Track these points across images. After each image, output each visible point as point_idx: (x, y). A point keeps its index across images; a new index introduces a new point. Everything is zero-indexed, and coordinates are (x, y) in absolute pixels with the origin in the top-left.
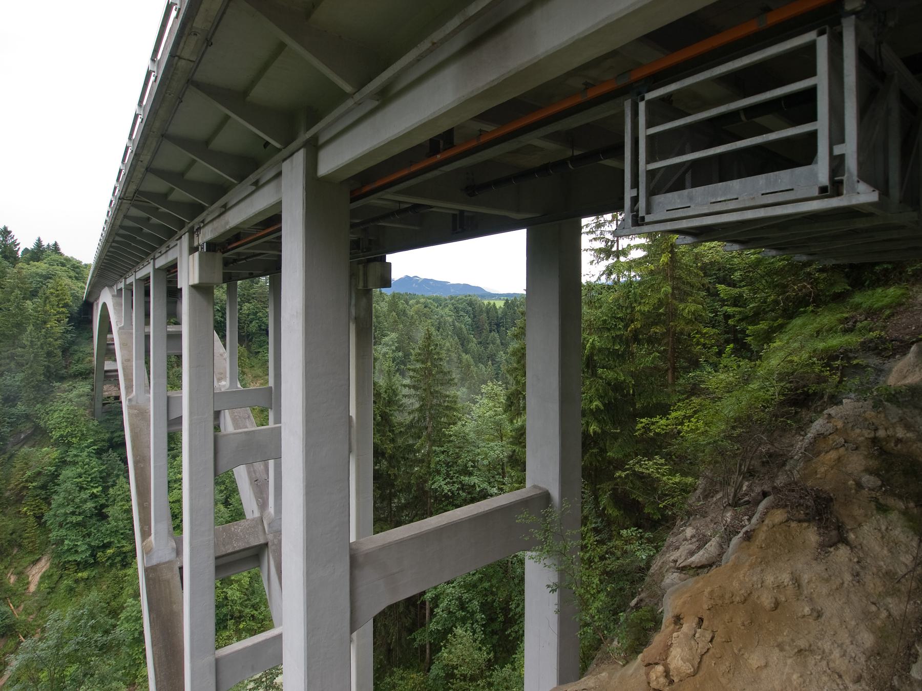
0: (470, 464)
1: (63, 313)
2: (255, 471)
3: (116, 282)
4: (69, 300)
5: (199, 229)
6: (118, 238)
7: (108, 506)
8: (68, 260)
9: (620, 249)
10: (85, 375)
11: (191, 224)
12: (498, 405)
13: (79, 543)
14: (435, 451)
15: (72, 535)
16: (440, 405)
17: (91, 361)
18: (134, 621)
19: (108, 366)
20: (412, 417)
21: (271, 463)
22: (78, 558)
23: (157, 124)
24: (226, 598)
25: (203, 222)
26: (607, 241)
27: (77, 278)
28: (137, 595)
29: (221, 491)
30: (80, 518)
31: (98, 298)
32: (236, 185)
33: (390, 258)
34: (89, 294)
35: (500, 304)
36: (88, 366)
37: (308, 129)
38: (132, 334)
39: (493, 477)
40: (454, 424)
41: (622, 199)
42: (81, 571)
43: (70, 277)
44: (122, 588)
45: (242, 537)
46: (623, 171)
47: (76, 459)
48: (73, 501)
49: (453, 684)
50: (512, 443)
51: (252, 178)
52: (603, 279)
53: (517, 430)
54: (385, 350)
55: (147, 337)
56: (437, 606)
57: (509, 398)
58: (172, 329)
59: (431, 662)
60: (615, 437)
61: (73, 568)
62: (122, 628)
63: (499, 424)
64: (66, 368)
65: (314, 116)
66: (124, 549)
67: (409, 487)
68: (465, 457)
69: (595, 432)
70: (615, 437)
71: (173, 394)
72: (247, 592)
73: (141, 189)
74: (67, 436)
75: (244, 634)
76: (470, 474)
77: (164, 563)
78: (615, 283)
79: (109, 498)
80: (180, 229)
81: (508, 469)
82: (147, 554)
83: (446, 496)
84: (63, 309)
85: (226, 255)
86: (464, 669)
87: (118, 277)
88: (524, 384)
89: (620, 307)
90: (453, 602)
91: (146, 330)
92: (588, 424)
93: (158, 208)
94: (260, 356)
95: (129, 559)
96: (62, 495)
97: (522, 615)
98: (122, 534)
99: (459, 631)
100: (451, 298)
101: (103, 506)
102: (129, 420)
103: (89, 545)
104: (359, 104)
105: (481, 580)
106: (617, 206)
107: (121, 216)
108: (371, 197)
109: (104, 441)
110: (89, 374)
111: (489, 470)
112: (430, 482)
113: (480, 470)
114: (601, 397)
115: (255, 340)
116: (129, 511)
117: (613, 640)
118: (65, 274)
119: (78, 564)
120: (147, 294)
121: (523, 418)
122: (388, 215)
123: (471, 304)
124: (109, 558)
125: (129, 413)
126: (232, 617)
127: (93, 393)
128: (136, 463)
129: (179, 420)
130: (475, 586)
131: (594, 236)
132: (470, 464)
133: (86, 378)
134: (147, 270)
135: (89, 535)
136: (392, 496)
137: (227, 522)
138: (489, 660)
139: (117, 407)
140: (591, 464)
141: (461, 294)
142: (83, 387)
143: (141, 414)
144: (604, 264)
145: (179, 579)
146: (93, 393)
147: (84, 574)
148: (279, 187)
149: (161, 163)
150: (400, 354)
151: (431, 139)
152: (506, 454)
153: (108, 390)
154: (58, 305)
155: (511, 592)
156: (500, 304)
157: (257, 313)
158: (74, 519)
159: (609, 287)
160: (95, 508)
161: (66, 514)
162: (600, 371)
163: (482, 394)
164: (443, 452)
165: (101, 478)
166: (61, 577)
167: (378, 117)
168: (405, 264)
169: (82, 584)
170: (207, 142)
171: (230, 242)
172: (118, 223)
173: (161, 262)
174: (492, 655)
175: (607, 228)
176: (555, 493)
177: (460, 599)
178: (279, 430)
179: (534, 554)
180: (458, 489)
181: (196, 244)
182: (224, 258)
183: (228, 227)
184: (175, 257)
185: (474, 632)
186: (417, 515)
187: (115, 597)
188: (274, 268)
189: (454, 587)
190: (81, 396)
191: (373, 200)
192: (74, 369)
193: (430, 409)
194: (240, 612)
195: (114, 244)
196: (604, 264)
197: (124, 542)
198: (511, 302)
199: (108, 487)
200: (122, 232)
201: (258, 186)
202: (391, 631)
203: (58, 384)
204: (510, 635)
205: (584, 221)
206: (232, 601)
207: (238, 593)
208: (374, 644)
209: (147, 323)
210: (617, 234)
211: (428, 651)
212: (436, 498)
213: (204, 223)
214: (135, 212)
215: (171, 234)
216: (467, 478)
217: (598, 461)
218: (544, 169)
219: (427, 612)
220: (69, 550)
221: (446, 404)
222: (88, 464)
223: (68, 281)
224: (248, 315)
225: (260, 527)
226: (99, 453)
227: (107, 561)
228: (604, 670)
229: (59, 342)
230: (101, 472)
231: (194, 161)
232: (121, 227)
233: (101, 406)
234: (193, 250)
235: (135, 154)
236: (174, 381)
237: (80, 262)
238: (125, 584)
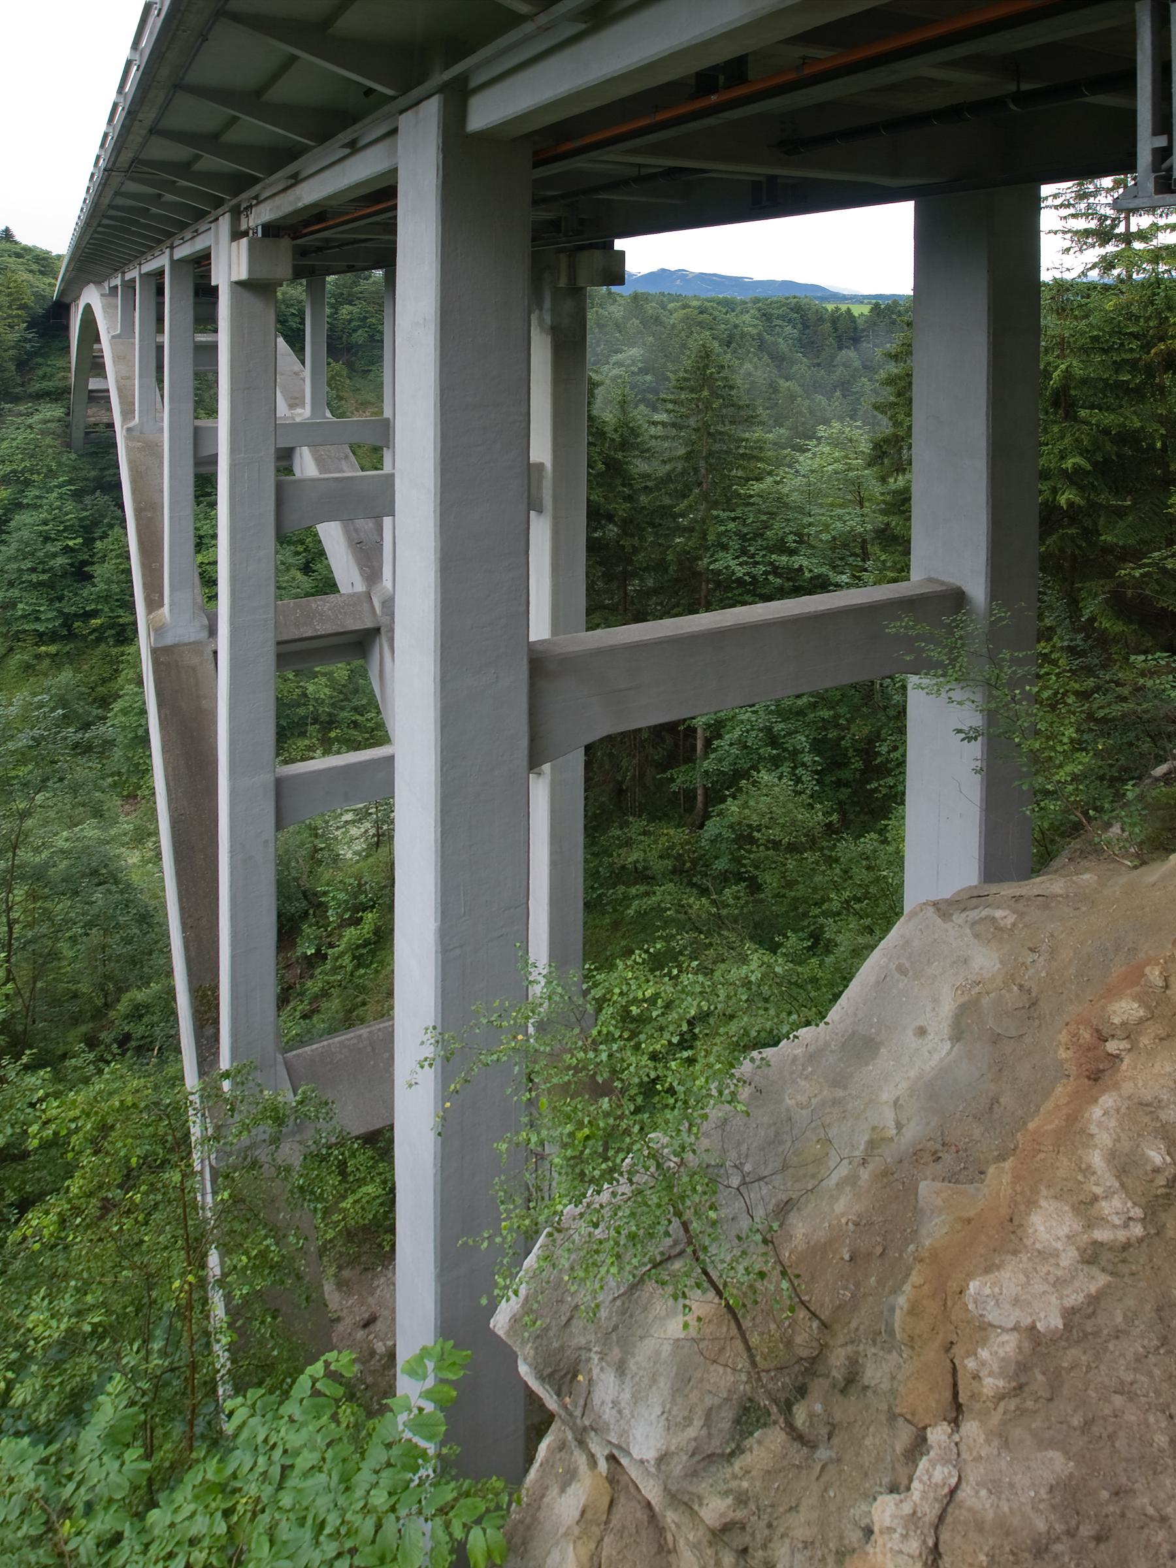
0: (791, 538)
1: (19, 316)
2: (356, 530)
3: (107, 277)
4: (29, 300)
5: (251, 207)
6: (106, 221)
7: (93, 563)
8: (27, 250)
9: (1134, 229)
10: (58, 395)
11: (234, 202)
12: (852, 456)
13: (42, 609)
14: (717, 517)
15: (32, 597)
16: (728, 452)
17: (65, 378)
18: (136, 714)
19: (94, 383)
20: (668, 467)
21: (387, 521)
22: (41, 628)
23: (165, 71)
24: (305, 695)
25: (256, 197)
26: (1102, 218)
27: (41, 273)
28: (140, 683)
29: (297, 553)
30: (45, 577)
31: (78, 297)
32: (314, 147)
33: (619, 244)
34: (62, 293)
35: (858, 310)
36: (61, 384)
37: (447, 67)
38: (134, 344)
39: (841, 559)
40: (759, 479)
41: (1133, 155)
42: (44, 643)
43: (31, 271)
44: (116, 671)
45: (325, 617)
46: (1134, 113)
47: (39, 502)
48: (33, 554)
49: (750, 852)
50: (884, 512)
51: (345, 137)
52: (1094, 275)
53: (895, 492)
54: (615, 372)
55: (160, 348)
56: (720, 737)
57: (877, 446)
58: (202, 338)
59: (706, 816)
60: (1120, 513)
61: (31, 640)
62: (116, 722)
63: (857, 484)
64: (22, 385)
65: (458, 47)
66: (121, 621)
67: (661, 566)
68: (778, 527)
69: (1071, 504)
70: (1120, 513)
71: (204, 423)
72: (344, 690)
73: (143, 156)
74: (23, 472)
75: (335, 747)
76: (792, 552)
77: (185, 644)
78: (1122, 281)
79: (95, 554)
80: (216, 209)
81: (874, 549)
82: (156, 630)
83: (740, 581)
84: (19, 312)
85: (298, 242)
86: (775, 833)
87: (110, 271)
88: (910, 428)
89: (1130, 317)
90: (754, 734)
91: (159, 339)
92: (1055, 491)
93: (175, 182)
94: (372, 376)
95: (129, 634)
96: (14, 546)
97: (902, 763)
98: (117, 600)
99: (765, 777)
100: (756, 301)
101: (85, 563)
102: (127, 455)
103: (60, 611)
104: (546, 29)
105: (814, 706)
106: (1123, 164)
107: (109, 193)
108: (577, 158)
109: (87, 480)
110: (63, 393)
111: (833, 549)
112: (706, 561)
113: (813, 547)
114: (1088, 451)
115: (356, 356)
116: (128, 572)
117: (1108, 825)
118: (22, 268)
119: (41, 635)
120: (160, 291)
121: (907, 476)
122: (620, 184)
123: (797, 308)
124: (94, 630)
125: (127, 447)
126: (316, 721)
127: (68, 419)
128: (138, 512)
129: (213, 460)
130: (801, 713)
131: (1072, 211)
132: (791, 538)
133: (56, 400)
134: (162, 261)
135: (60, 599)
136: (625, 578)
137: (307, 595)
138: (829, 825)
139: (108, 437)
140: (1062, 550)
141: (780, 295)
142: (51, 412)
143: (148, 449)
144: (1094, 254)
145: (213, 665)
146: (68, 419)
147: (52, 649)
148: (393, 151)
149: (173, 122)
150: (649, 378)
151: (697, 73)
152: (869, 527)
153: (94, 415)
154: (10, 307)
155: (881, 728)
156: (865, 309)
157: (366, 318)
158: (34, 577)
159: (1106, 288)
160: (72, 565)
161: (20, 570)
162: (1083, 413)
163: (819, 439)
164: (734, 519)
165: (81, 527)
166: (11, 649)
167: (587, 45)
168: (644, 254)
169: (47, 661)
170: (259, 93)
171: (306, 223)
172: (106, 201)
173: (183, 251)
174: (835, 817)
175: (1103, 199)
176: (977, 590)
177: (768, 730)
178: (393, 475)
179: (926, 681)
180: (766, 573)
181: (244, 227)
182: (295, 246)
183: (300, 205)
184: (207, 244)
185: (798, 780)
186: (678, 605)
187: (104, 681)
188: (387, 259)
189: (753, 712)
190: (46, 422)
191: (580, 163)
192: (36, 387)
193: (706, 458)
194: (330, 714)
195: (100, 229)
196: (1094, 254)
197: (121, 612)
198: (885, 310)
199: (94, 539)
200: (112, 212)
201: (354, 148)
202: (624, 764)
203: (8, 406)
204: (876, 790)
205: (1046, 190)
206: (316, 700)
207: (327, 691)
208: (587, 779)
209: (160, 330)
210: (1125, 208)
211: (700, 798)
212: (718, 584)
213: (258, 200)
214: (132, 187)
215: (200, 215)
216: (784, 558)
217: (1079, 547)
218: (953, 113)
219: (700, 744)
220: (24, 617)
221: (741, 451)
222: (60, 508)
223: (27, 276)
224: (350, 321)
225: (366, 605)
226: (78, 495)
227: (90, 633)
228: (1087, 870)
229: (12, 352)
230: (81, 520)
231: (235, 119)
232: (110, 206)
233: (82, 435)
234: (236, 235)
235: (129, 112)
236: (205, 404)
237: (48, 252)
238: (121, 666)
